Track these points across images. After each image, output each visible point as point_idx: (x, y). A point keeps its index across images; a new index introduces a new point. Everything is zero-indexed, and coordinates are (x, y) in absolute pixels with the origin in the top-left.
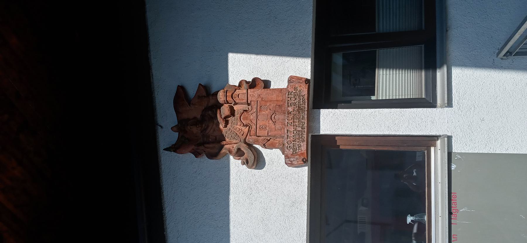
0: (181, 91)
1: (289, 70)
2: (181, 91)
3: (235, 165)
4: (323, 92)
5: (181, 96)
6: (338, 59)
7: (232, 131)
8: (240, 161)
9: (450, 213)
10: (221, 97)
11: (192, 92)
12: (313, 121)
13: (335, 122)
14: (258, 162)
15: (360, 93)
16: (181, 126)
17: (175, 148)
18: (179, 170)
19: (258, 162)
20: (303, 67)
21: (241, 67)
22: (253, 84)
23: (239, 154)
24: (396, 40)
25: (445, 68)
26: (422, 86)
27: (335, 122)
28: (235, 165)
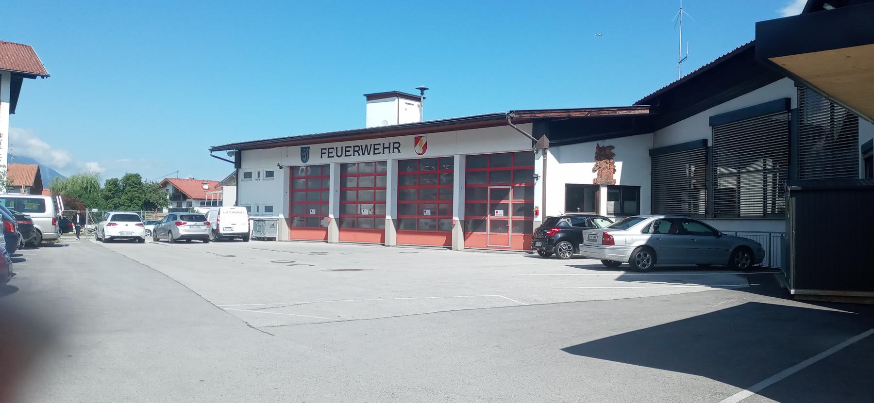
0: (613, 147)
1: (617, 179)
2: (613, 147)
3: (593, 165)
4: (611, 188)
5: (612, 147)
6: (617, 191)
7: (603, 163)
8: (120, 178)
10: (58, 228)
11: (613, 151)
12: (604, 186)
13: (604, 192)
14: (594, 171)
15: (610, 197)
16: (604, 148)
17: (598, 146)
18: (591, 147)
19: (594, 171)
20: (618, 183)
21: (619, 165)
23: (596, 166)
24: (622, 208)
27: (604, 192)
28: (593, 165)
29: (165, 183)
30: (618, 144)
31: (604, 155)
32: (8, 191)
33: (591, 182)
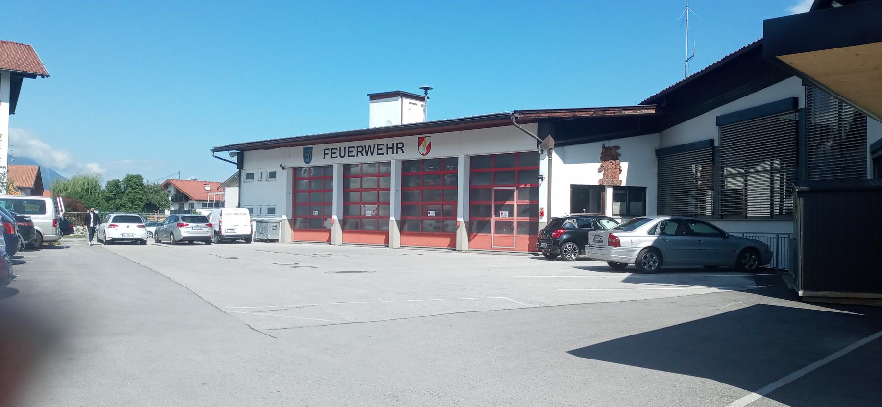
1: (623, 179)
3: (598, 165)
4: (617, 189)
5: (618, 148)
7: (608, 164)
9: (797, 151)
11: (618, 151)
12: (610, 186)
13: (609, 193)
14: (600, 171)
15: (616, 198)
16: (610, 149)
18: (596, 148)
19: (600, 171)
20: (624, 184)
21: (624, 166)
22: (621, 171)
23: (602, 166)
24: (628, 209)
25: (547, 158)
26: (346, 190)
27: (609, 193)
28: (598, 165)
30: (624, 144)
31: (610, 156)
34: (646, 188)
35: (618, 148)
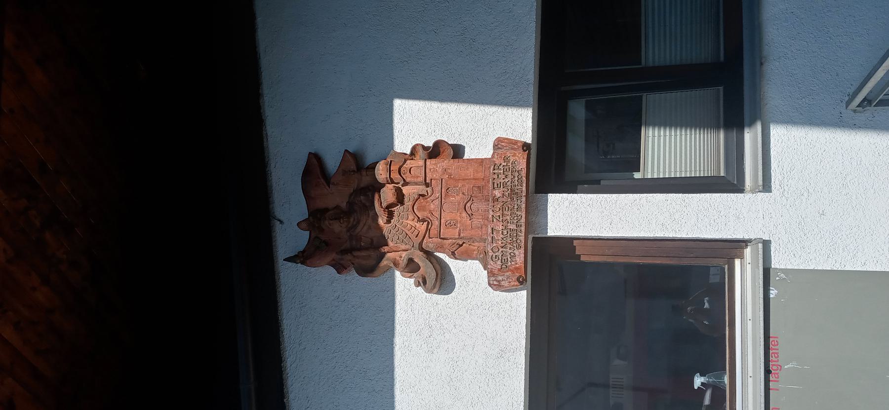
1: (496, 127)
3: (404, 286)
4: (553, 165)
5: (314, 170)
6: (578, 110)
7: (399, 230)
9: (768, 372)
11: (332, 163)
12: (535, 213)
13: (572, 215)
14: (442, 282)
15: (615, 166)
16: (316, 219)
17: (303, 258)
18: (309, 294)
19: (442, 282)
20: (519, 123)
21: (415, 122)
22: (435, 151)
23: (411, 267)
24: (678, 77)
27: (572, 215)
28: (404, 286)
29: (414, 149)
30: (296, 130)
31: (350, 217)
32: (370, 256)
33: (519, 301)
34: (771, 192)
35: (314, 170)
